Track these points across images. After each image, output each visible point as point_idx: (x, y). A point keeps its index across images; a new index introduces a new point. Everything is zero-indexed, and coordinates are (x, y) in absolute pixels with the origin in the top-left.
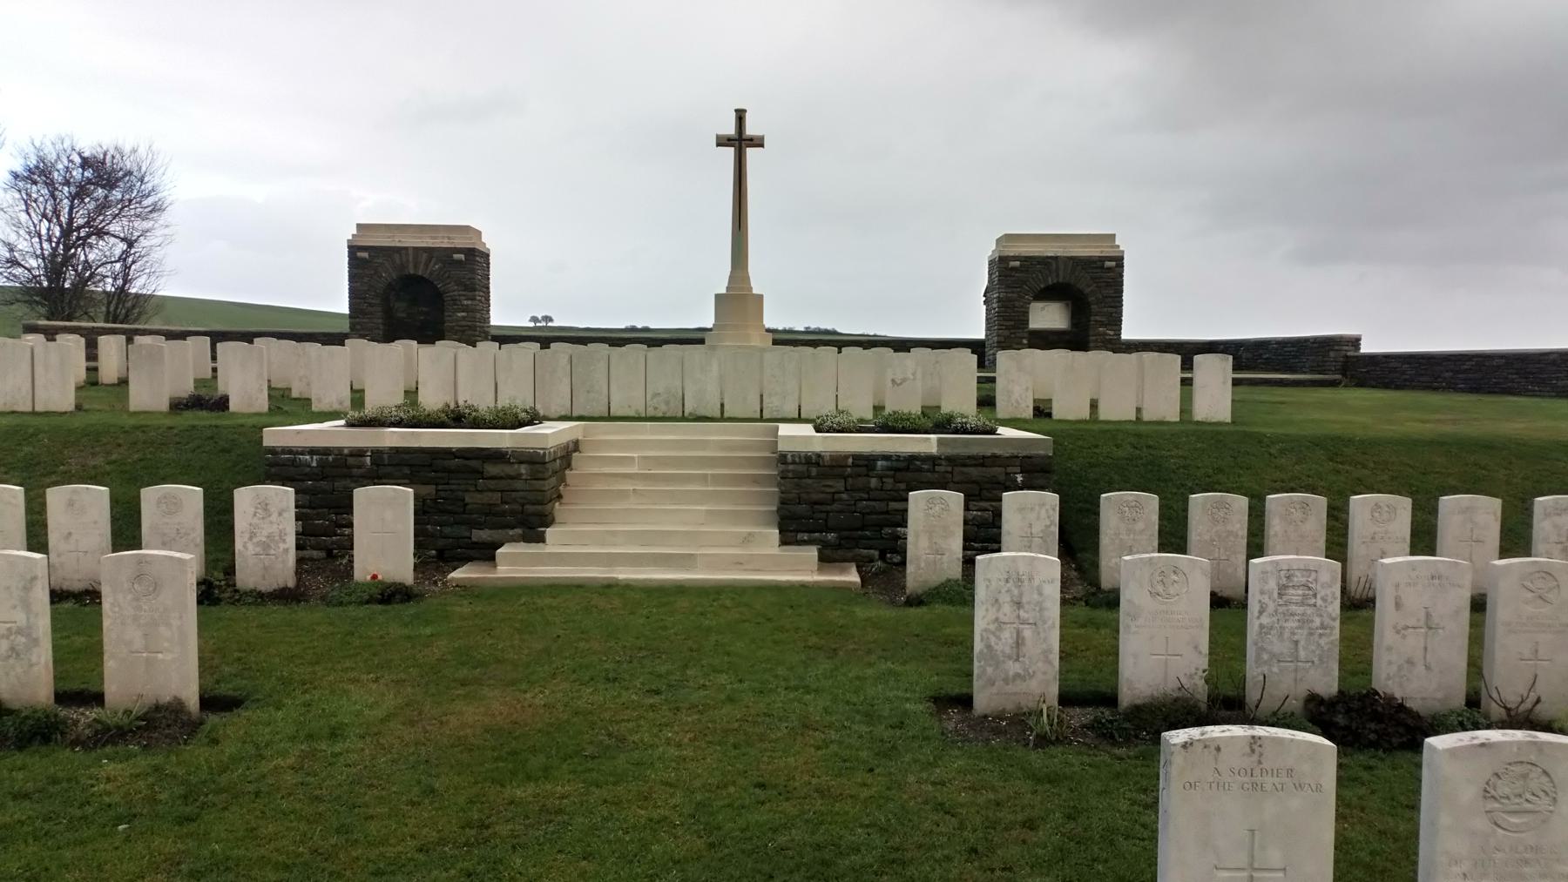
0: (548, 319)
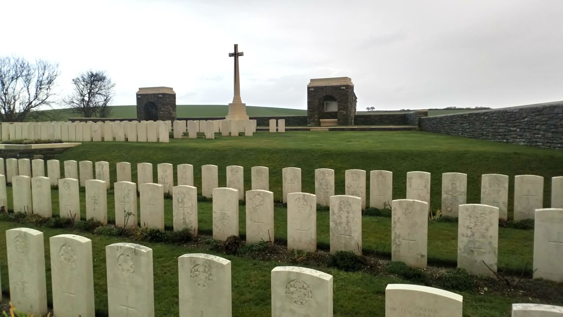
0: (373, 108)
